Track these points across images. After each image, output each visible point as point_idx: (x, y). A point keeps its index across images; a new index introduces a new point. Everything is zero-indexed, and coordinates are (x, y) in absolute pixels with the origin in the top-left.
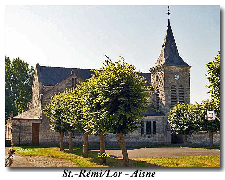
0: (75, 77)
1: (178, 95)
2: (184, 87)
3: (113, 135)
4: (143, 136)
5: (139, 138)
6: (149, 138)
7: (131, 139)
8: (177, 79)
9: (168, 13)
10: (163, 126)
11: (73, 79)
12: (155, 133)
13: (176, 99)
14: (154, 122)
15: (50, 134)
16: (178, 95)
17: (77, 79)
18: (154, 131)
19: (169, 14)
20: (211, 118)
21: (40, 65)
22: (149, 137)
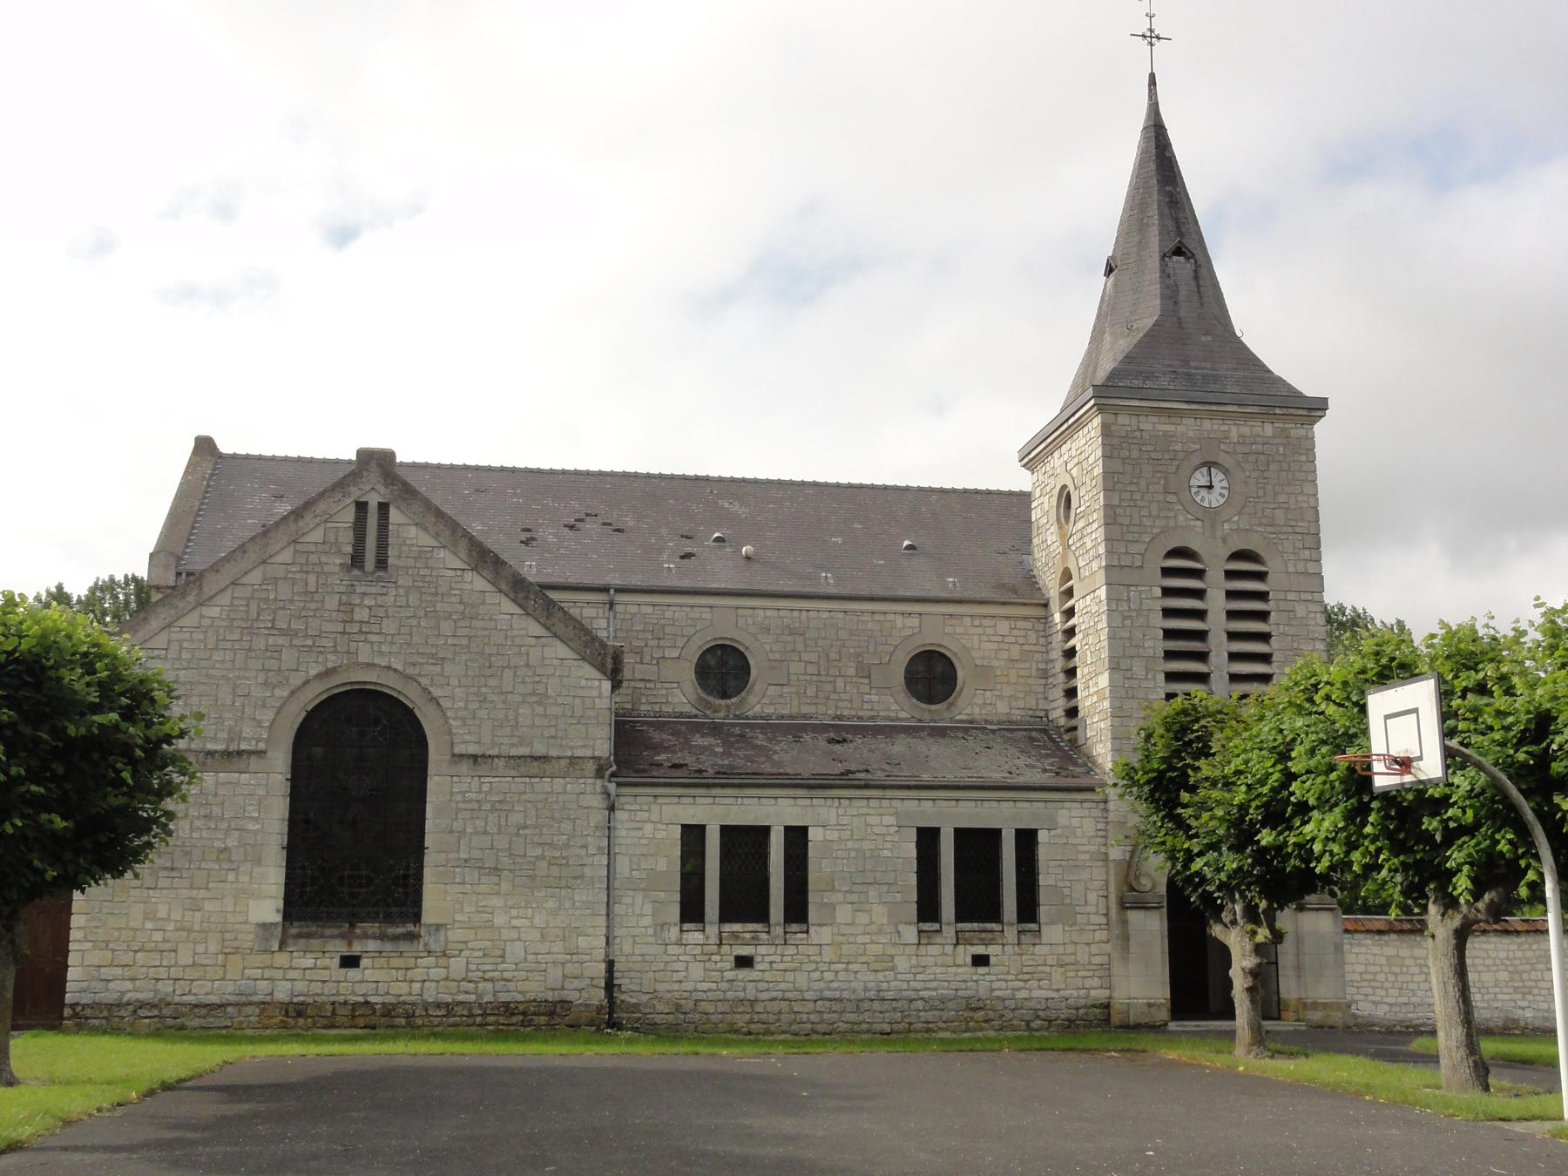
0: (373, 500)
1: (1217, 624)
2: (1273, 565)
3: (679, 943)
4: (933, 950)
5: (902, 963)
6: (982, 970)
7: (829, 976)
8: (1214, 499)
9: (1144, 29)
10: (1098, 873)
11: (361, 507)
12: (1033, 926)
13: (1202, 657)
14: (1027, 840)
15: (158, 936)
16: (1217, 624)
17: (394, 515)
18: (1028, 910)
19: (1151, 37)
20: (1405, 764)
21: (225, 447)
22: (744, 962)
